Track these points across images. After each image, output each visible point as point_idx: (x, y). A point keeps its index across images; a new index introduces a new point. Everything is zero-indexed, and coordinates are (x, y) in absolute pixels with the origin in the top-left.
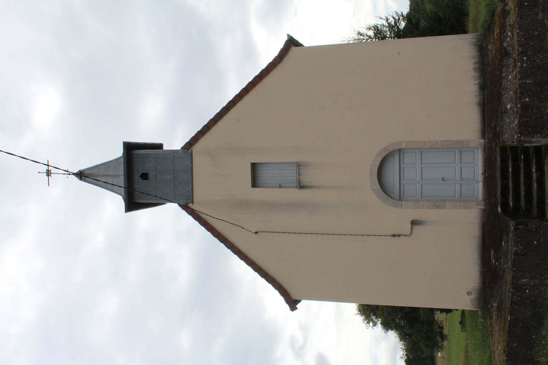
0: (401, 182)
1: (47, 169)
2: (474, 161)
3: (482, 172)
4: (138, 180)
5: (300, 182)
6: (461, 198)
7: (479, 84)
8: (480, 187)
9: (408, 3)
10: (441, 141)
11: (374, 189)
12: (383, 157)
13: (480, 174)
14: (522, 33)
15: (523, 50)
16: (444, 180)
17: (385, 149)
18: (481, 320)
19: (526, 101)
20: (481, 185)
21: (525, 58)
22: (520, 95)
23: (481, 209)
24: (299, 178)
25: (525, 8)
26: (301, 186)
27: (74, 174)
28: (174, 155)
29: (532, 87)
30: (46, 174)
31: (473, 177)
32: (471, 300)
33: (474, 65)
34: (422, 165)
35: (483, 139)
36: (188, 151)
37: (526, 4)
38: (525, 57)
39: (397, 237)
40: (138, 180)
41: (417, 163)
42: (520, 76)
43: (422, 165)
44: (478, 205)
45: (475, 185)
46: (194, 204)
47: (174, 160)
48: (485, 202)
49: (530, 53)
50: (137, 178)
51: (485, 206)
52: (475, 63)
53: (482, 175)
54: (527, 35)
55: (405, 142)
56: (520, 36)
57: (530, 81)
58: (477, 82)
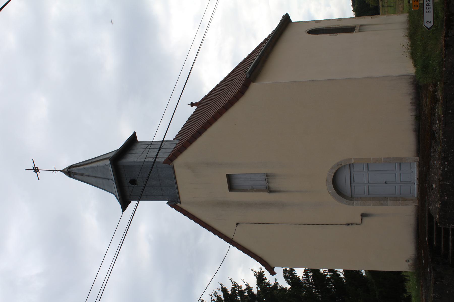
0: (352, 185)
1: (34, 166)
2: (411, 169)
3: (417, 178)
4: (128, 184)
5: (269, 187)
6: (400, 195)
7: (415, 115)
8: (415, 188)
9: (351, 2)
10: (383, 158)
11: (330, 192)
12: (336, 170)
13: (416, 179)
14: (445, 140)
15: (445, 156)
16: (386, 182)
17: (338, 164)
18: (416, 287)
19: (445, 199)
20: (416, 186)
21: (446, 163)
22: (441, 194)
23: (415, 206)
24: (268, 185)
25: (449, 116)
26: (270, 191)
27: (61, 171)
28: (157, 166)
29: (450, 188)
30: (34, 171)
31: (410, 181)
32: (409, 265)
33: (411, 101)
34: (368, 172)
35: (418, 157)
36: (169, 165)
37: (450, 111)
38: (447, 162)
39: (350, 226)
40: (128, 184)
41: (365, 170)
42: (441, 178)
43: (368, 172)
44: (413, 203)
45: (412, 186)
46: (182, 204)
47: (157, 170)
48: (419, 201)
49: (450, 159)
50: (126, 183)
51: (419, 203)
52: (412, 99)
53: (417, 180)
54: (449, 142)
55: (353, 159)
56: (443, 142)
57: (449, 183)
58: (414, 113)
